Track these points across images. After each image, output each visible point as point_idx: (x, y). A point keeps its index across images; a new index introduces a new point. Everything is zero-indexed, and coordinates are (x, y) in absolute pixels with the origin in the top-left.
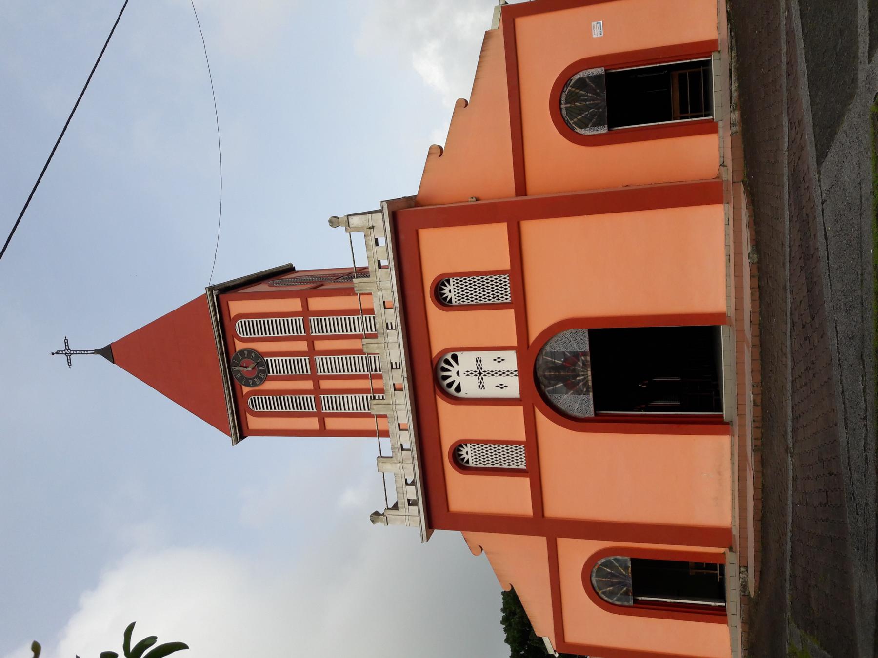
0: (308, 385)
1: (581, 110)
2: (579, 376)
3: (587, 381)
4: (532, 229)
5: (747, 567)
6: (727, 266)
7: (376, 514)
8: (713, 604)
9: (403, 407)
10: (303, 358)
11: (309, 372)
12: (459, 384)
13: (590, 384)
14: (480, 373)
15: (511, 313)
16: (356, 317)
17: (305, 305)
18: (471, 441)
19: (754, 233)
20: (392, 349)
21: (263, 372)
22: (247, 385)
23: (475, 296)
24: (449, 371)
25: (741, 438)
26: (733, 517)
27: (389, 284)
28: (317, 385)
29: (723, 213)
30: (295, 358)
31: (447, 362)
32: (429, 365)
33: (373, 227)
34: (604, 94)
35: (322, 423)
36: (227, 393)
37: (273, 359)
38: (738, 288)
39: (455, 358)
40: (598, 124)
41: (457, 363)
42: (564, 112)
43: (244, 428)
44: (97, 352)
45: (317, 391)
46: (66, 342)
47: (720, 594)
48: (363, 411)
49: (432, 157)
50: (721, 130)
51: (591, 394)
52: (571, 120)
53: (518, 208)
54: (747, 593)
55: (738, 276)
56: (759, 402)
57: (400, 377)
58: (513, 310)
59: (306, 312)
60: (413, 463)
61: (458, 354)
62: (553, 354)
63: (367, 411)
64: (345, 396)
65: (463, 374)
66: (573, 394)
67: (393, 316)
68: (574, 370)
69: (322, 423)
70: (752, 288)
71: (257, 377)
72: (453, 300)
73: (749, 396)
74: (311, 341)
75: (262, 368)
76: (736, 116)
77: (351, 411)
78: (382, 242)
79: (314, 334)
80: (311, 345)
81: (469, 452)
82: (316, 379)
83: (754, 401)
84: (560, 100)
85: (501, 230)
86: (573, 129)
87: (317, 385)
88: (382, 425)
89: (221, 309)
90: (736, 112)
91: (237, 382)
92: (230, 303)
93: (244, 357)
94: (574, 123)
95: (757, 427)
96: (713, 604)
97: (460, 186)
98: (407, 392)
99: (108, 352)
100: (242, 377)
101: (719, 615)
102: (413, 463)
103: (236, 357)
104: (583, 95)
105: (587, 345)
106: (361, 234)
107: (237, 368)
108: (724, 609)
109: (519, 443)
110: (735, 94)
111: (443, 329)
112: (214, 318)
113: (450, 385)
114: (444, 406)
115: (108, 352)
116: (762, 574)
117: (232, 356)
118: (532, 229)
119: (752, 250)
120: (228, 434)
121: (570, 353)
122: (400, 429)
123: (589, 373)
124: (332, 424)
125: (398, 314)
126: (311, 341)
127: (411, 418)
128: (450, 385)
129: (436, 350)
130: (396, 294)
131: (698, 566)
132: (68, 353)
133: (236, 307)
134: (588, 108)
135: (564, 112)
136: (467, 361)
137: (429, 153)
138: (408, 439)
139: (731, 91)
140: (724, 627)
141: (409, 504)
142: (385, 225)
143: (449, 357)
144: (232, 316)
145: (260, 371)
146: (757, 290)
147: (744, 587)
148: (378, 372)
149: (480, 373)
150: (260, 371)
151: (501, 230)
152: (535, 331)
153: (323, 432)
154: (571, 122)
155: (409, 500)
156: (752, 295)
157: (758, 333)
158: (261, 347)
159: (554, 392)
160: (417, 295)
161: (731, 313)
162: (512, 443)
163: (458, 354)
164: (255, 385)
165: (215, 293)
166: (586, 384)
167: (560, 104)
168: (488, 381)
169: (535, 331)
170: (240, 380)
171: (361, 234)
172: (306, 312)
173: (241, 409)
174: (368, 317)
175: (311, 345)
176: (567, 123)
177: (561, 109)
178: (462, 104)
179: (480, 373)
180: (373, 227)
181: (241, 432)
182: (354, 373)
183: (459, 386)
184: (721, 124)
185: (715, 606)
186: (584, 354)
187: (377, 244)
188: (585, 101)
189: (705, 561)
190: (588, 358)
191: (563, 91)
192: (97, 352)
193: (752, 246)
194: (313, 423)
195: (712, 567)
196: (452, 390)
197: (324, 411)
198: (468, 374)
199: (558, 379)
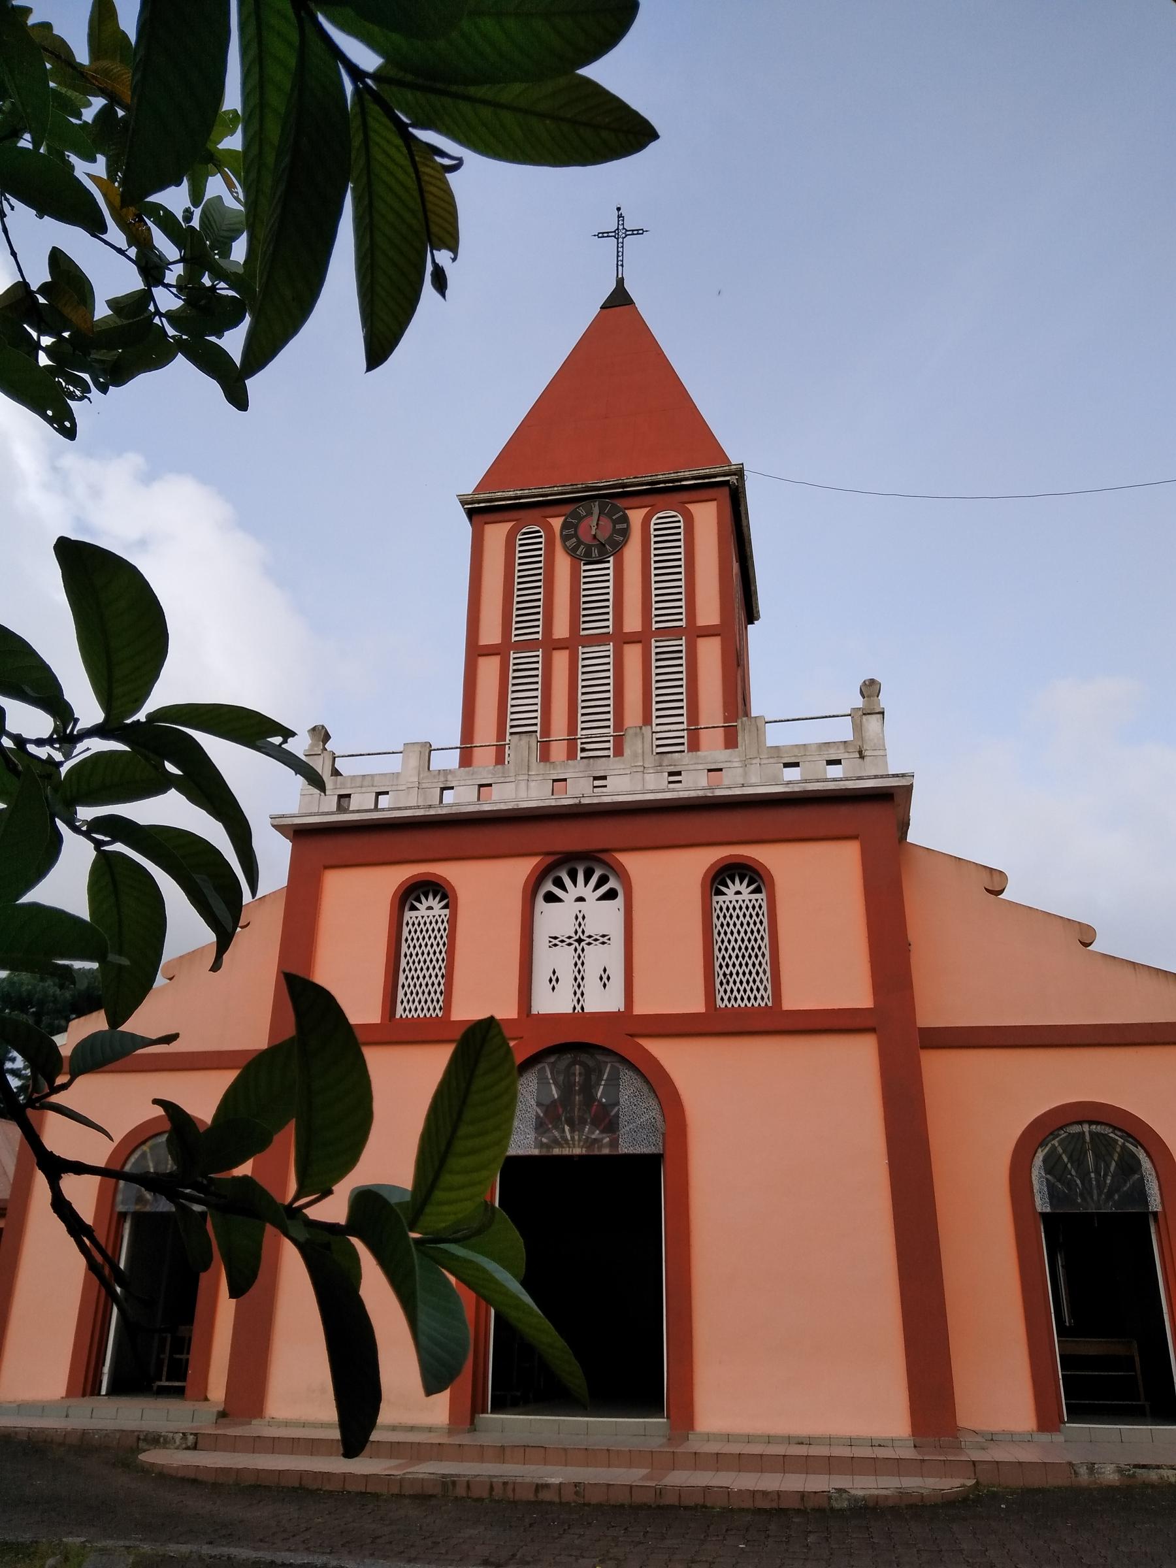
0: (561, 630)
1: (1078, 1160)
2: (572, 1131)
3: (561, 1146)
4: (861, 1054)
5: (195, 1447)
6: (789, 1440)
7: (327, 737)
8: (106, 1369)
9: (523, 794)
10: (610, 623)
11: (583, 633)
12: (559, 900)
13: (556, 1151)
14: (579, 940)
15: (697, 1006)
16: (684, 719)
17: (708, 632)
18: (453, 921)
19: (890, 1503)
20: (629, 783)
21: (588, 553)
22: (565, 526)
23: (730, 939)
24: (586, 883)
25: (436, 1451)
26: (287, 1424)
27: (754, 779)
28: (560, 645)
29: (894, 1435)
30: (610, 610)
31: (603, 881)
32: (601, 847)
33: (862, 757)
34: (1109, 1208)
35: (490, 651)
36: (553, 489)
37: (611, 571)
38: (741, 1462)
39: (611, 895)
40: (1053, 1195)
41: (599, 899)
42: (1075, 1129)
43: (487, 517)
44: (620, 282)
45: (550, 645)
46: (639, 232)
47: (122, 1386)
48: (509, 724)
49: (985, 875)
50: (1045, 1437)
51: (536, 1152)
52: (1060, 1143)
53: (900, 1033)
54: (142, 1445)
55: (806, 1465)
56: (546, 1496)
57: (579, 790)
58: (703, 1010)
59: (694, 633)
60: (418, 807)
61: (619, 901)
62: (614, 1080)
63: (509, 730)
64: (538, 693)
65: (580, 907)
66: (538, 1117)
67: (694, 784)
68: (583, 1122)
69: (490, 651)
70: (779, 1494)
71: (579, 543)
72: (720, 898)
73: (556, 1475)
74: (642, 638)
75: (595, 553)
76: (1109, 1475)
77: (510, 702)
78: (834, 772)
79: (654, 644)
80: (633, 639)
81: (430, 912)
82: (572, 644)
83: (547, 1486)
84: (1097, 1123)
85: (856, 993)
86: (1042, 1144)
87: (560, 645)
88: (484, 756)
89: (703, 488)
90: (1116, 1477)
91: (568, 509)
92: (715, 503)
93: (615, 522)
94: (1054, 1148)
95: (492, 1488)
96: (106, 1369)
97: (932, 922)
98: (553, 803)
99: (620, 298)
100: (581, 519)
101: (85, 1383)
102: (418, 807)
103: (616, 510)
104: (1108, 1166)
105: (631, 1151)
106: (848, 735)
107: (596, 510)
108: (96, 1391)
109: (447, 1007)
110: (1153, 1476)
111: (669, 877)
112: (687, 474)
113: (559, 883)
114: (522, 869)
115: (620, 298)
116: (192, 1481)
117: (620, 503)
118: (861, 1054)
119: (856, 1499)
120: (480, 487)
121: (617, 1116)
122: (481, 786)
123: (577, 1151)
124: (489, 668)
125: (701, 793)
126: (642, 638)
127: (503, 807)
128: (559, 883)
129: (629, 861)
130: (738, 792)
131: (182, 1345)
132: (620, 233)
133: (707, 516)
134: (1084, 1176)
135: (1075, 1129)
136: (605, 917)
137: (992, 870)
138: (461, 799)
139: (1158, 1467)
140: (61, 1390)
141: (341, 797)
142: (869, 778)
143: (612, 884)
144: (689, 506)
145: (589, 548)
146: (775, 1505)
147: (156, 1440)
148: (580, 755)
149: (580, 941)
150: (589, 548)
151: (856, 993)
152: (663, 1051)
153: (475, 651)
154: (1055, 1142)
155: (349, 796)
156: (765, 1494)
157: (687, 1502)
158: (632, 553)
159: (542, 1081)
160: (738, 830)
161: (694, 1445)
162: (448, 993)
163: (619, 901)
164: (565, 538)
165: (733, 479)
166: (556, 1142)
167: (1091, 1123)
168: (563, 959)
169: (663, 1051)
170: (574, 515)
171: (848, 735)
172: (694, 633)
173: (522, 514)
174: (685, 740)
175: (633, 639)
176: (1053, 1134)
177: (1080, 1123)
178: (1085, 936)
179: (579, 940)
180: (862, 757)
181: (479, 512)
182: (581, 711)
183: (557, 899)
184: (1058, 1438)
185: (101, 1374)
186: (614, 1143)
187: (830, 762)
188: (1097, 1173)
189: (194, 1357)
190: (606, 1151)
191: (1115, 1128)
192: (620, 282)
193: (864, 1498)
194: (491, 635)
195: (179, 1370)
196: (549, 886)
197: (512, 656)
198: (580, 919)
199: (567, 1090)
